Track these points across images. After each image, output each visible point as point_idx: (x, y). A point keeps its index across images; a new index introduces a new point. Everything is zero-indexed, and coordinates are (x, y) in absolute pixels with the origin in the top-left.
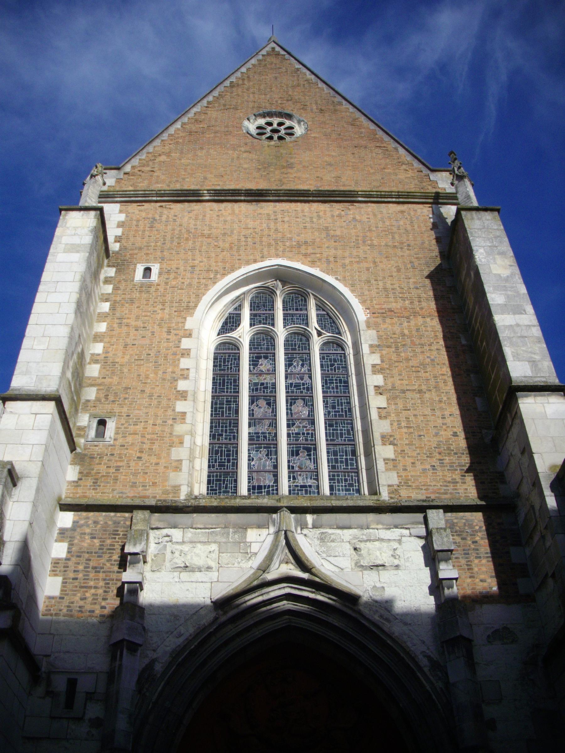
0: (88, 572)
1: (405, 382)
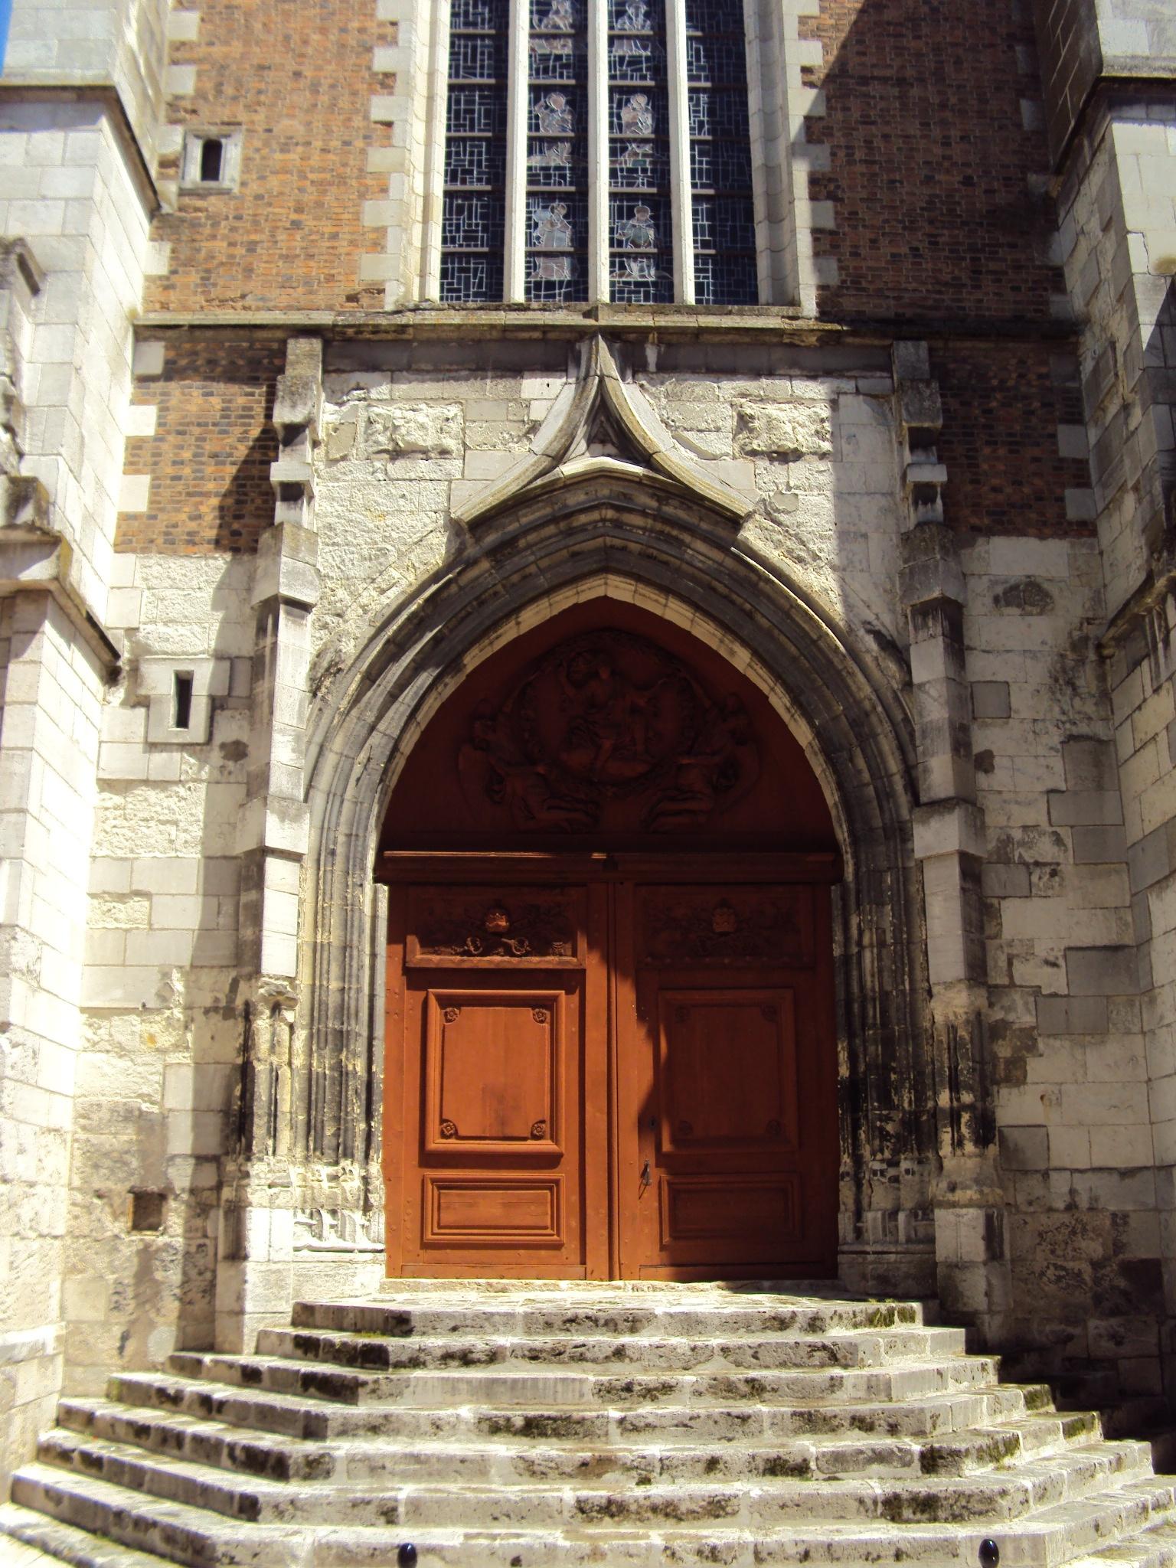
0: (203, 463)
1: (869, 60)
